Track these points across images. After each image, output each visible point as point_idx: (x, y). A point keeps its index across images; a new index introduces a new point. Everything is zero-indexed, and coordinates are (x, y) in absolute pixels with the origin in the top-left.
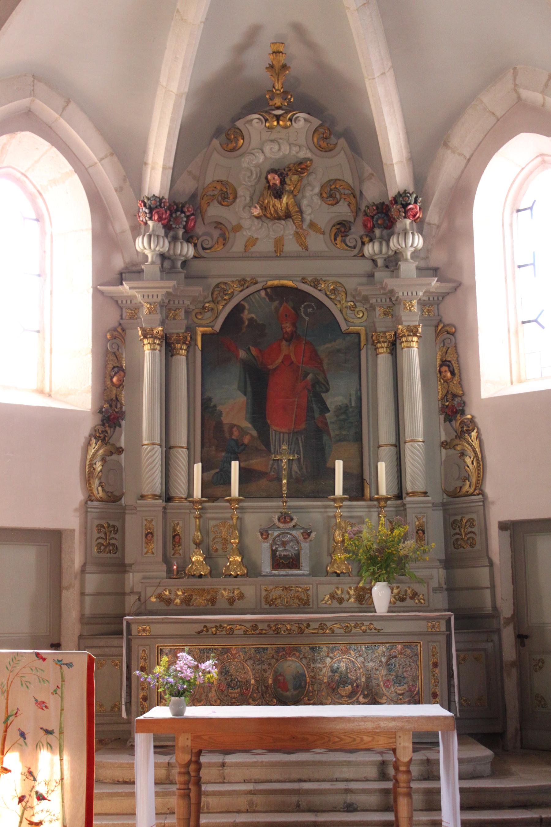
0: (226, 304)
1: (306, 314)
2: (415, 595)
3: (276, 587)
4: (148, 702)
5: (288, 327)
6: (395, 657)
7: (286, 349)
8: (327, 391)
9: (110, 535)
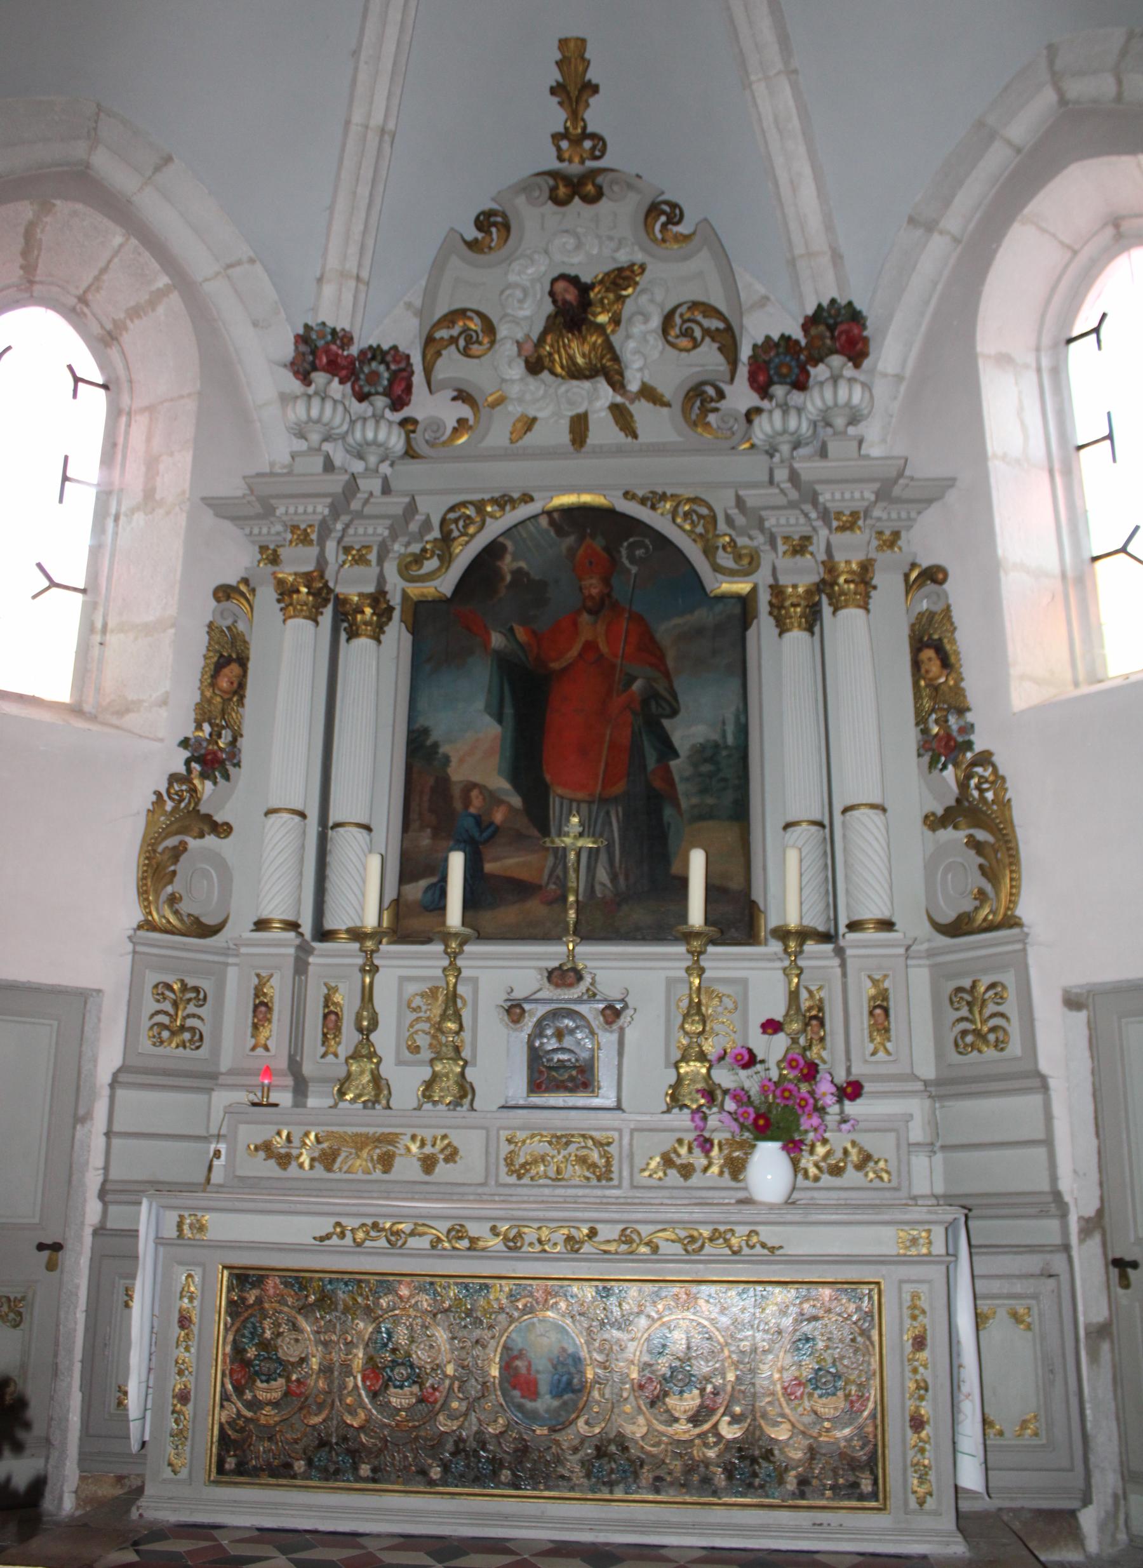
0: (467, 543)
1: (632, 559)
2: (866, 1159)
4: (190, 1406)
5: (593, 586)
6: (815, 1318)
7: (589, 628)
8: (674, 712)
9: (185, 1008)
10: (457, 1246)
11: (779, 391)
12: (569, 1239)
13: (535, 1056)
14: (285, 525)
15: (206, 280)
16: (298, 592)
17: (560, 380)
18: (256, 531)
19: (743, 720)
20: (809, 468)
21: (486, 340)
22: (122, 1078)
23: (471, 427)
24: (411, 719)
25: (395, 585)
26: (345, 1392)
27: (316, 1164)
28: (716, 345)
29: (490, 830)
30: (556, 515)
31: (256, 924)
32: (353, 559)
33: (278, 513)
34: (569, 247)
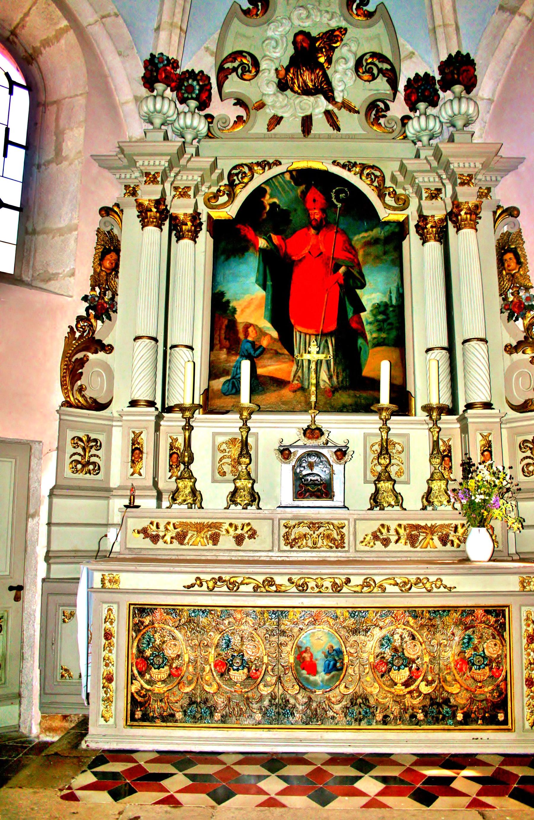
3: (299, 524)
4: (113, 683)
9: (90, 451)
10: (269, 589)
11: (422, 106)
12: (334, 584)
13: (298, 478)
14: (142, 172)
15: (90, 25)
16: (151, 211)
17: (297, 95)
18: (123, 176)
19: (401, 291)
20: (446, 148)
21: (253, 71)
22: (56, 492)
23: (244, 121)
24: (214, 287)
25: (203, 209)
26: (205, 673)
27: (174, 541)
28: (385, 79)
29: (260, 350)
30: (294, 173)
31: (130, 403)
32: (180, 194)
33: (138, 165)
34: (304, 16)
